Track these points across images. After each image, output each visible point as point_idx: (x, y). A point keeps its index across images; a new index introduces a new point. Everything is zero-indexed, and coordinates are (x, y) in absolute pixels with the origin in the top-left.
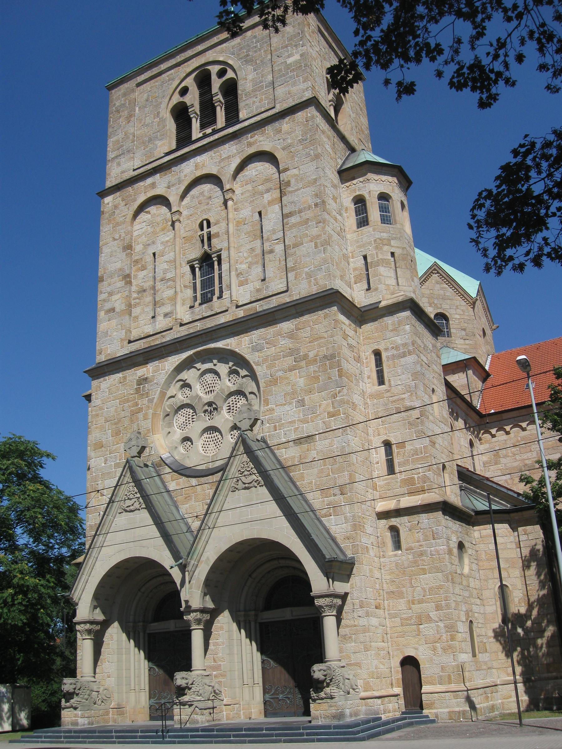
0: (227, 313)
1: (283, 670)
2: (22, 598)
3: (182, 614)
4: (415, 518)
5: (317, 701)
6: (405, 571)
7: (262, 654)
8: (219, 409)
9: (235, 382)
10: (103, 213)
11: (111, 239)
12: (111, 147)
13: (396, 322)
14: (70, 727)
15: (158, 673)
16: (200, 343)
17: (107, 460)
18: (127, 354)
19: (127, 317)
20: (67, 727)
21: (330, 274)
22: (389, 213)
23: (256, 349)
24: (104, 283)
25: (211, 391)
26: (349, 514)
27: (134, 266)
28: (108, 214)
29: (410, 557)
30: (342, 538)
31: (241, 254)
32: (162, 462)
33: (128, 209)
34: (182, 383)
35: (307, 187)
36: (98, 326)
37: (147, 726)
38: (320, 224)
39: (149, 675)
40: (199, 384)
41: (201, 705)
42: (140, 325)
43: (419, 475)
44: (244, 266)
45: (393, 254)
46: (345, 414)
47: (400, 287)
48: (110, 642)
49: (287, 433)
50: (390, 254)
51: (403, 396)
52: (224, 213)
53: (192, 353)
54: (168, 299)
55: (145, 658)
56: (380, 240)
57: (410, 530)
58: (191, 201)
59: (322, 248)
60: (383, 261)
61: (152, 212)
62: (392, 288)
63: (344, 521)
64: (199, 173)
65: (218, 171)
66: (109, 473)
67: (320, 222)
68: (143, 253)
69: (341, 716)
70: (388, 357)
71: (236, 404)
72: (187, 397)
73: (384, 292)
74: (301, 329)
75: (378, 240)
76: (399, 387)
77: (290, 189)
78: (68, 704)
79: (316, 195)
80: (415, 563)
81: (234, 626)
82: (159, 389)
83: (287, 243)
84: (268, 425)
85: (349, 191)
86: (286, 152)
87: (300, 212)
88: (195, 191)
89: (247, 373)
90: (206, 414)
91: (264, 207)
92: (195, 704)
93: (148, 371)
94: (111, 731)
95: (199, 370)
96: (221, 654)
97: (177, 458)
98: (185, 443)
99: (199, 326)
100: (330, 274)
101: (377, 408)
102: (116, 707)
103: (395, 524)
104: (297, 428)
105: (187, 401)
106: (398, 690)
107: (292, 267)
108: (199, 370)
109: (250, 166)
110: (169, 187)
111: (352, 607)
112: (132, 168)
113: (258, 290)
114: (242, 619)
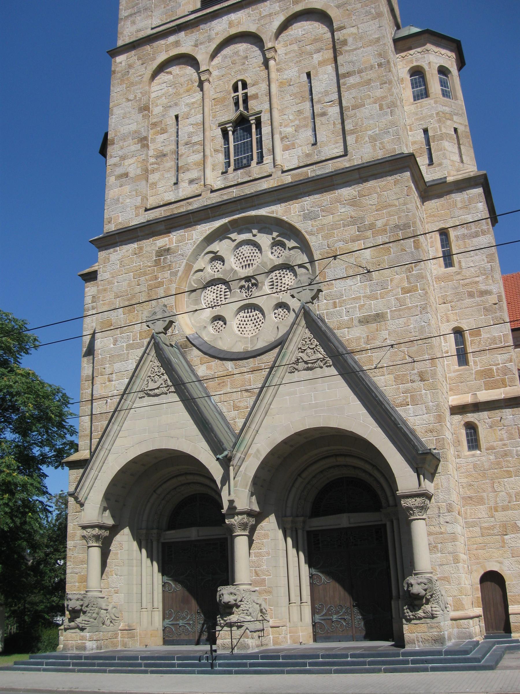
0: (270, 178)
1: (337, 585)
2: (8, 498)
3: (223, 517)
4: (497, 414)
5: (413, 622)
6: (485, 473)
7: (310, 567)
8: (260, 285)
9: (280, 255)
10: (114, 72)
11: (124, 100)
12: (125, 5)
13: (466, 199)
14: (75, 652)
15: (174, 589)
16: (238, 210)
17: (117, 341)
18: (144, 223)
19: (144, 182)
20: (71, 652)
21: (399, 138)
22: (448, 88)
23: (308, 217)
24: (115, 146)
25: (249, 265)
26: (431, 403)
27: (151, 129)
28: (120, 74)
29: (492, 457)
30: (423, 431)
31: (286, 117)
32: (189, 343)
33: (146, 68)
34: (212, 255)
35: (367, 46)
36: (106, 192)
37: (158, 651)
38: (385, 85)
39: (163, 591)
40: (233, 257)
41: (252, 626)
42: (159, 193)
43: (498, 366)
44: (290, 130)
45: (456, 130)
46: (424, 290)
47: (465, 165)
48: (119, 552)
49: (350, 310)
50: (453, 130)
51: (477, 279)
52: (264, 73)
53: (227, 221)
54: (195, 164)
55: (159, 571)
56: (443, 113)
57: (491, 427)
58: (223, 61)
59: (389, 110)
60: (447, 136)
61: (174, 72)
62: (457, 164)
63: (425, 411)
64: (233, 31)
65: (258, 29)
66: (121, 355)
67: (385, 83)
68: (163, 116)
69: (440, 640)
70: (457, 237)
71: (281, 279)
72: (218, 271)
73: (450, 168)
74: (365, 196)
75: (441, 113)
76: (472, 269)
77: (347, 48)
78: (73, 623)
79: (380, 55)
80: (498, 465)
81: (280, 534)
82: (185, 261)
83: (344, 104)
84: (325, 301)
85: (404, 62)
86: (341, 10)
87: (360, 72)
88: (227, 51)
89: (297, 245)
90: (243, 291)
91: (314, 68)
92: (246, 625)
93: (171, 241)
94: (136, 658)
95: (234, 241)
96: (265, 567)
97: (206, 339)
98: (215, 322)
99: (235, 193)
100: (399, 138)
101: (446, 292)
102: (127, 628)
103: (472, 420)
104: (364, 305)
105: (217, 275)
106: (479, 611)
107: (351, 130)
108: (234, 241)
109: (295, 25)
110: (196, 46)
111: (437, 512)
112: (150, 27)
113: (308, 155)
114: (288, 526)
